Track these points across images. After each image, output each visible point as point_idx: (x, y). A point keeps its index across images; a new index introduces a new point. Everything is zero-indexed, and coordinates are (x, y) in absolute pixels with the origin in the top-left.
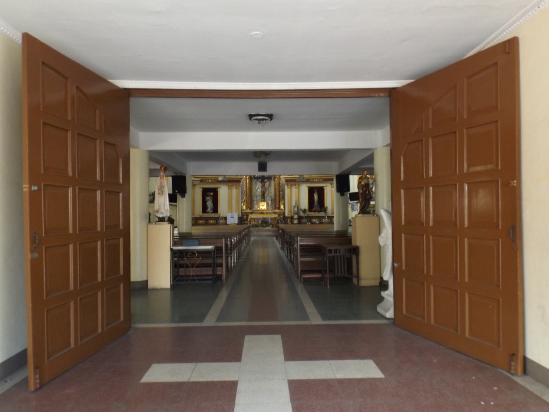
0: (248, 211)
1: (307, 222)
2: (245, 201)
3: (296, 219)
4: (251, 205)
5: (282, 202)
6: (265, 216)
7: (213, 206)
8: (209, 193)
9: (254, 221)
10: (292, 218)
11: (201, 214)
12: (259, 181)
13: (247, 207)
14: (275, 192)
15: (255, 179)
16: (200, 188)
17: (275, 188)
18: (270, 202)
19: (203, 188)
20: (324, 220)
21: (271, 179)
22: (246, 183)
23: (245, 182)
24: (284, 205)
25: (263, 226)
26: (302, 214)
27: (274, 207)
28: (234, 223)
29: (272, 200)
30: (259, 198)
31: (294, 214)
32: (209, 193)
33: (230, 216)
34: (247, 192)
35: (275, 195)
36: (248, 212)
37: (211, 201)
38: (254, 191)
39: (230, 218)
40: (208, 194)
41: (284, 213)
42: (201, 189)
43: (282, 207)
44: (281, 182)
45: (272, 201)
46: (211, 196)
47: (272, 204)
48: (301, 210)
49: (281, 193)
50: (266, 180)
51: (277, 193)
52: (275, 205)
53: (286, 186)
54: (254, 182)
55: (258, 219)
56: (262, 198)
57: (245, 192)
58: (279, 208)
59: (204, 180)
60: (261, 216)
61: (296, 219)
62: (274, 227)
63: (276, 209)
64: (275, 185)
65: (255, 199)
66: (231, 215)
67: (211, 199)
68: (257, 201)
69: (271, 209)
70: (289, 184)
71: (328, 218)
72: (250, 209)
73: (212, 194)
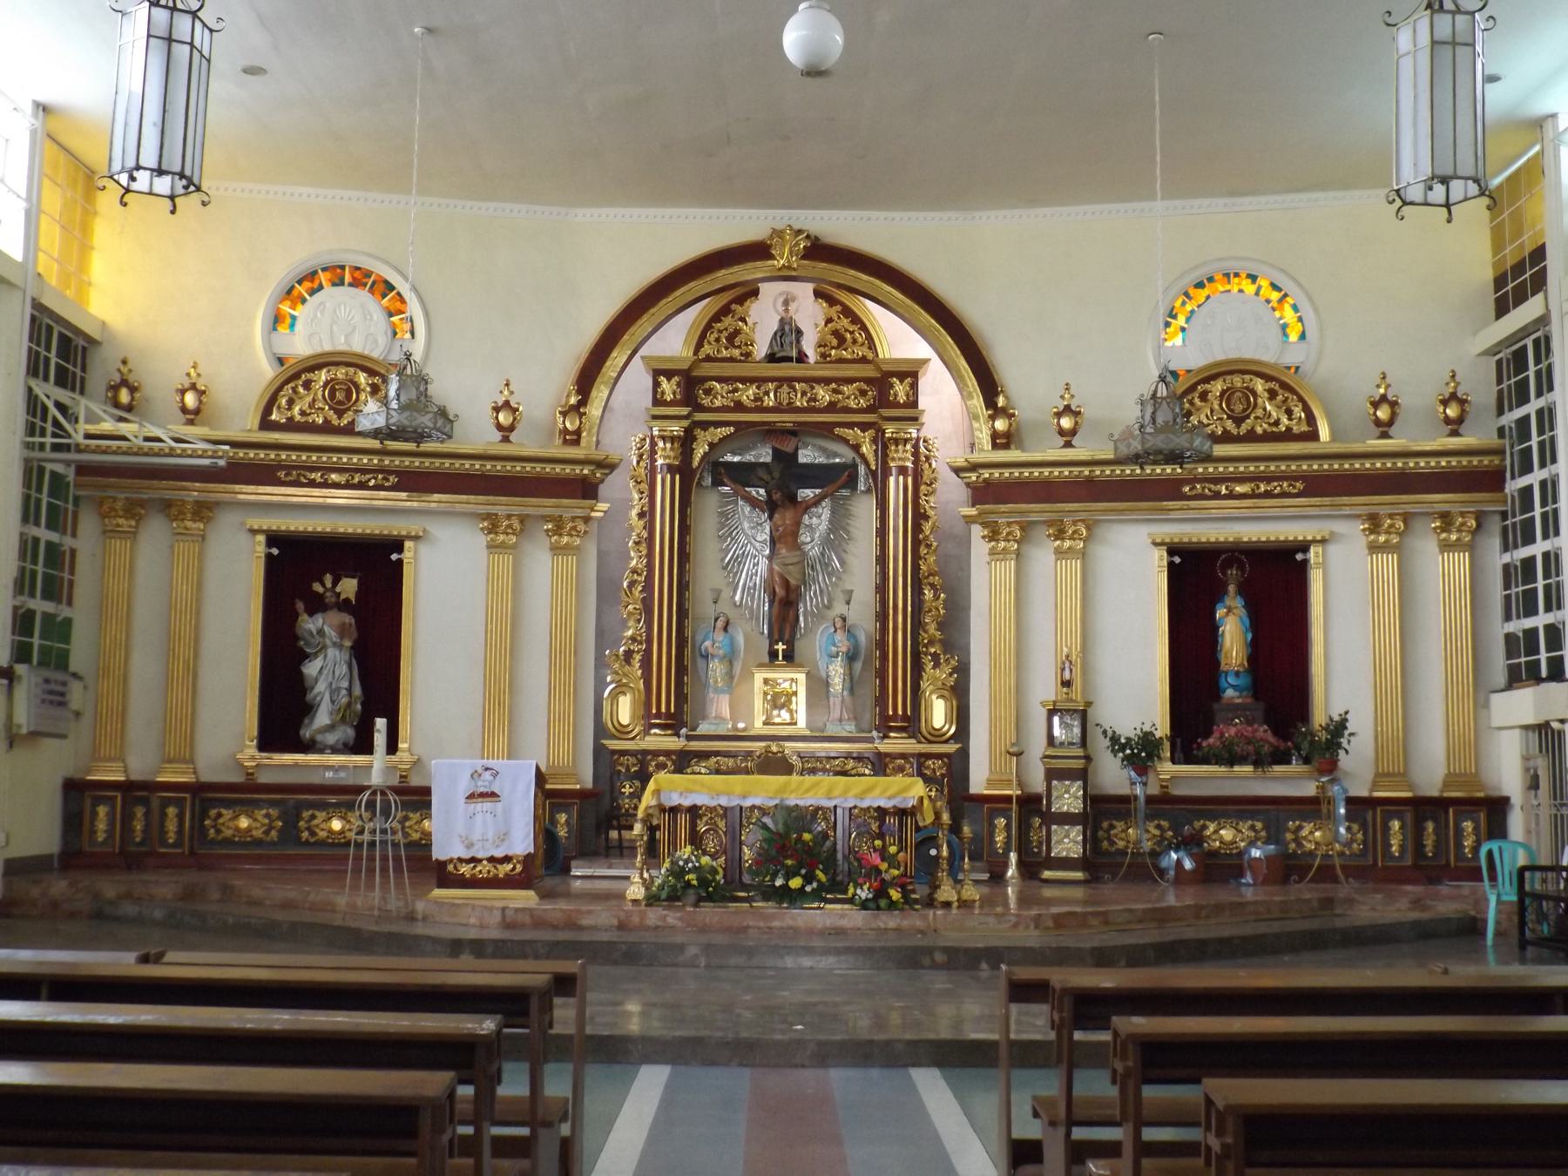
0: (659, 740)
1: (1163, 846)
2: (629, 654)
3: (1067, 819)
4: (681, 697)
5: (935, 675)
6: (804, 792)
7: (357, 691)
8: (328, 580)
9: (695, 840)
10: (1031, 806)
11: (250, 753)
12: (753, 503)
13: (647, 716)
14: (881, 589)
15: (717, 483)
16: (254, 532)
17: (882, 560)
18: (836, 673)
19: (273, 539)
20: (1307, 828)
21: (852, 483)
22: (647, 515)
23: (637, 501)
24: (959, 694)
25: (786, 896)
26: (1113, 776)
27: (869, 715)
28: (499, 854)
29: (851, 658)
30: (751, 633)
31: (1052, 774)
32: (328, 580)
33: (464, 786)
34: (648, 587)
35: (882, 616)
36: (656, 753)
37: (340, 647)
38: (708, 575)
39: (463, 800)
40: (317, 587)
41: (958, 765)
42: (261, 538)
43: (938, 713)
44: (930, 504)
45: (858, 666)
46: (344, 606)
47: (852, 684)
48: (1116, 743)
49: (928, 594)
50: (806, 493)
51: (899, 595)
52: (881, 700)
53: (979, 547)
54: (709, 504)
55: (736, 817)
56: (773, 642)
57: (632, 584)
58: (912, 724)
59: (289, 468)
60: (762, 791)
61: (1067, 819)
62: (892, 905)
63: (885, 728)
64: (882, 533)
65: (714, 642)
66: (475, 775)
67: (342, 631)
68: (730, 659)
69: (849, 729)
70: (1004, 513)
71: (1349, 817)
72: (674, 723)
73: (349, 587)
